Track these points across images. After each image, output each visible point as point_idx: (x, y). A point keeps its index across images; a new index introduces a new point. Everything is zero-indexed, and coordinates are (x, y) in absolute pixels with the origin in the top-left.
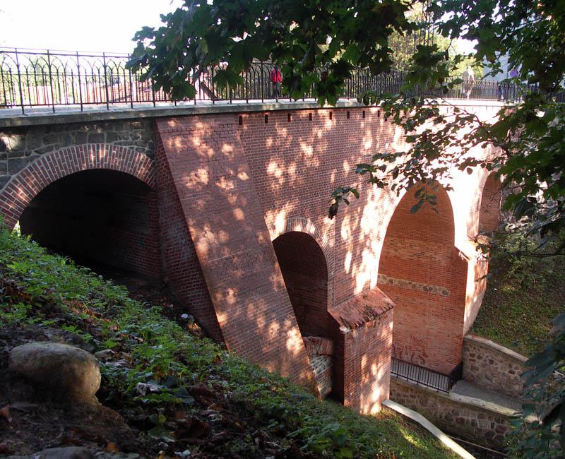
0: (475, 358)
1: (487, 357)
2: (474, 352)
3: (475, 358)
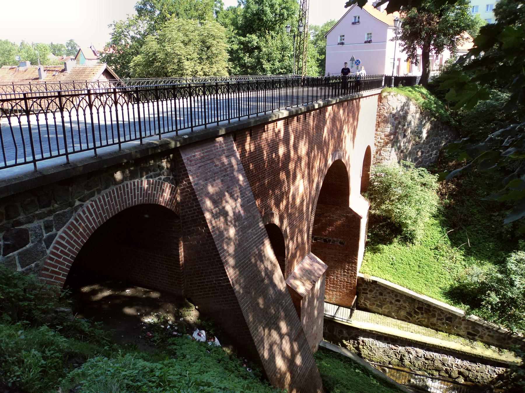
0: (368, 292)
1: (377, 290)
2: (366, 287)
3: (368, 292)
